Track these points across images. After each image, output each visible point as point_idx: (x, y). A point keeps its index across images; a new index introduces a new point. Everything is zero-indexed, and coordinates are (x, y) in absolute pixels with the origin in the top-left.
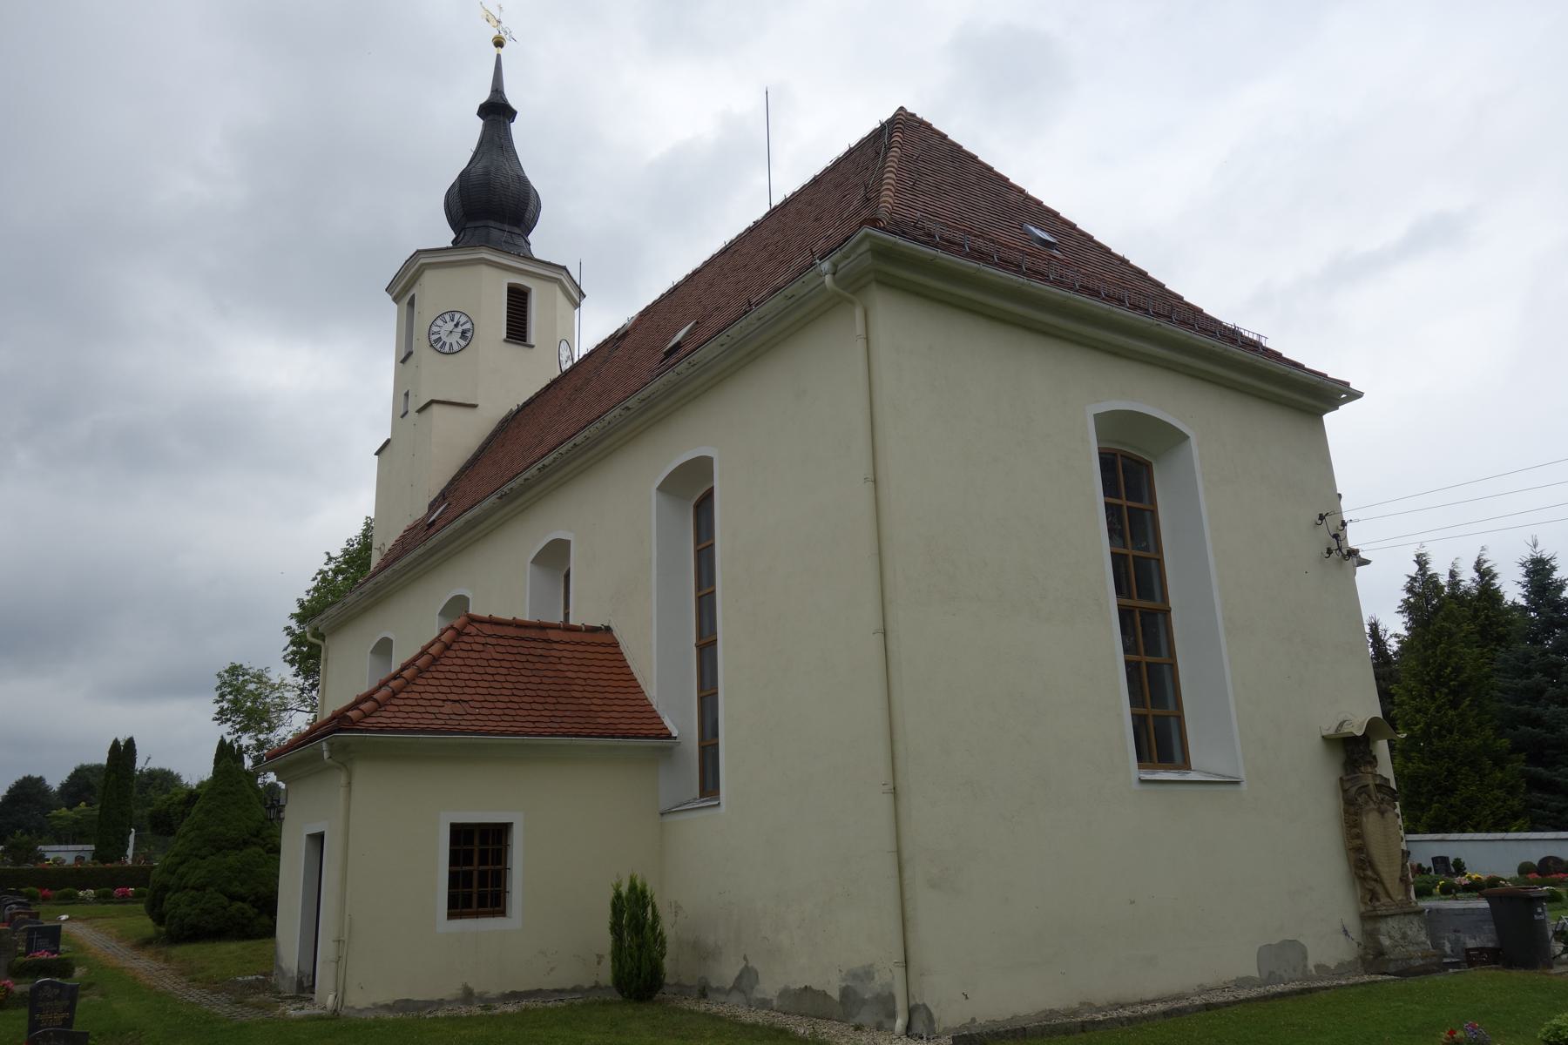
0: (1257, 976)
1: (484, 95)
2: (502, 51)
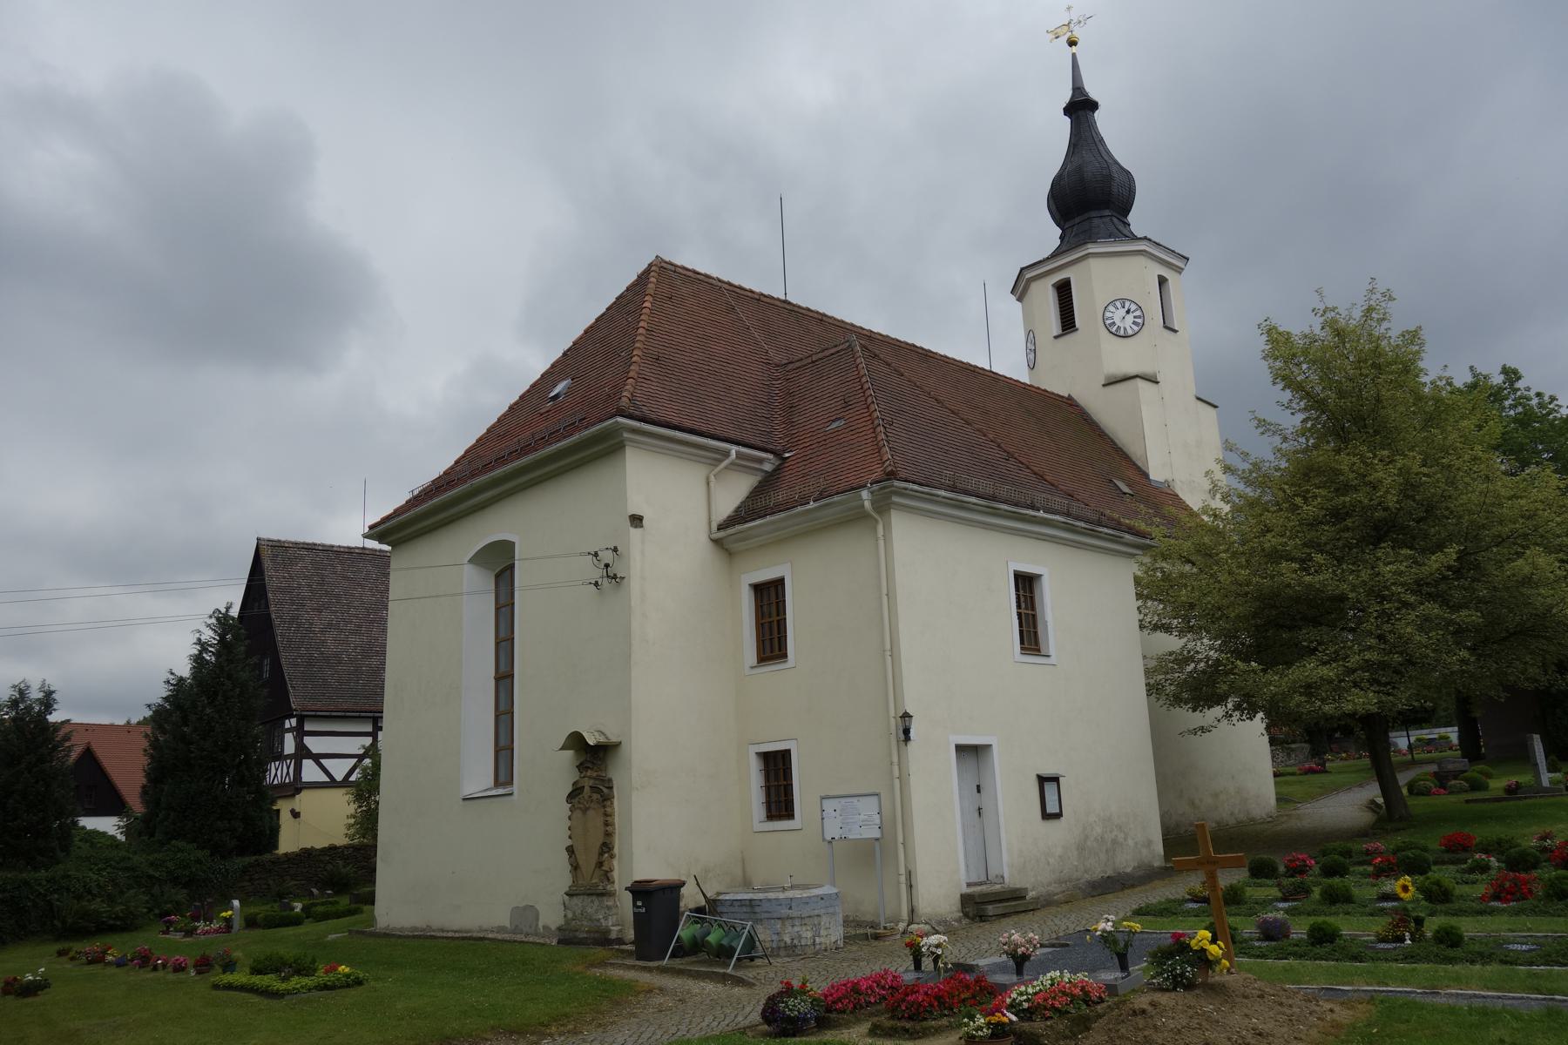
1: (1066, 95)
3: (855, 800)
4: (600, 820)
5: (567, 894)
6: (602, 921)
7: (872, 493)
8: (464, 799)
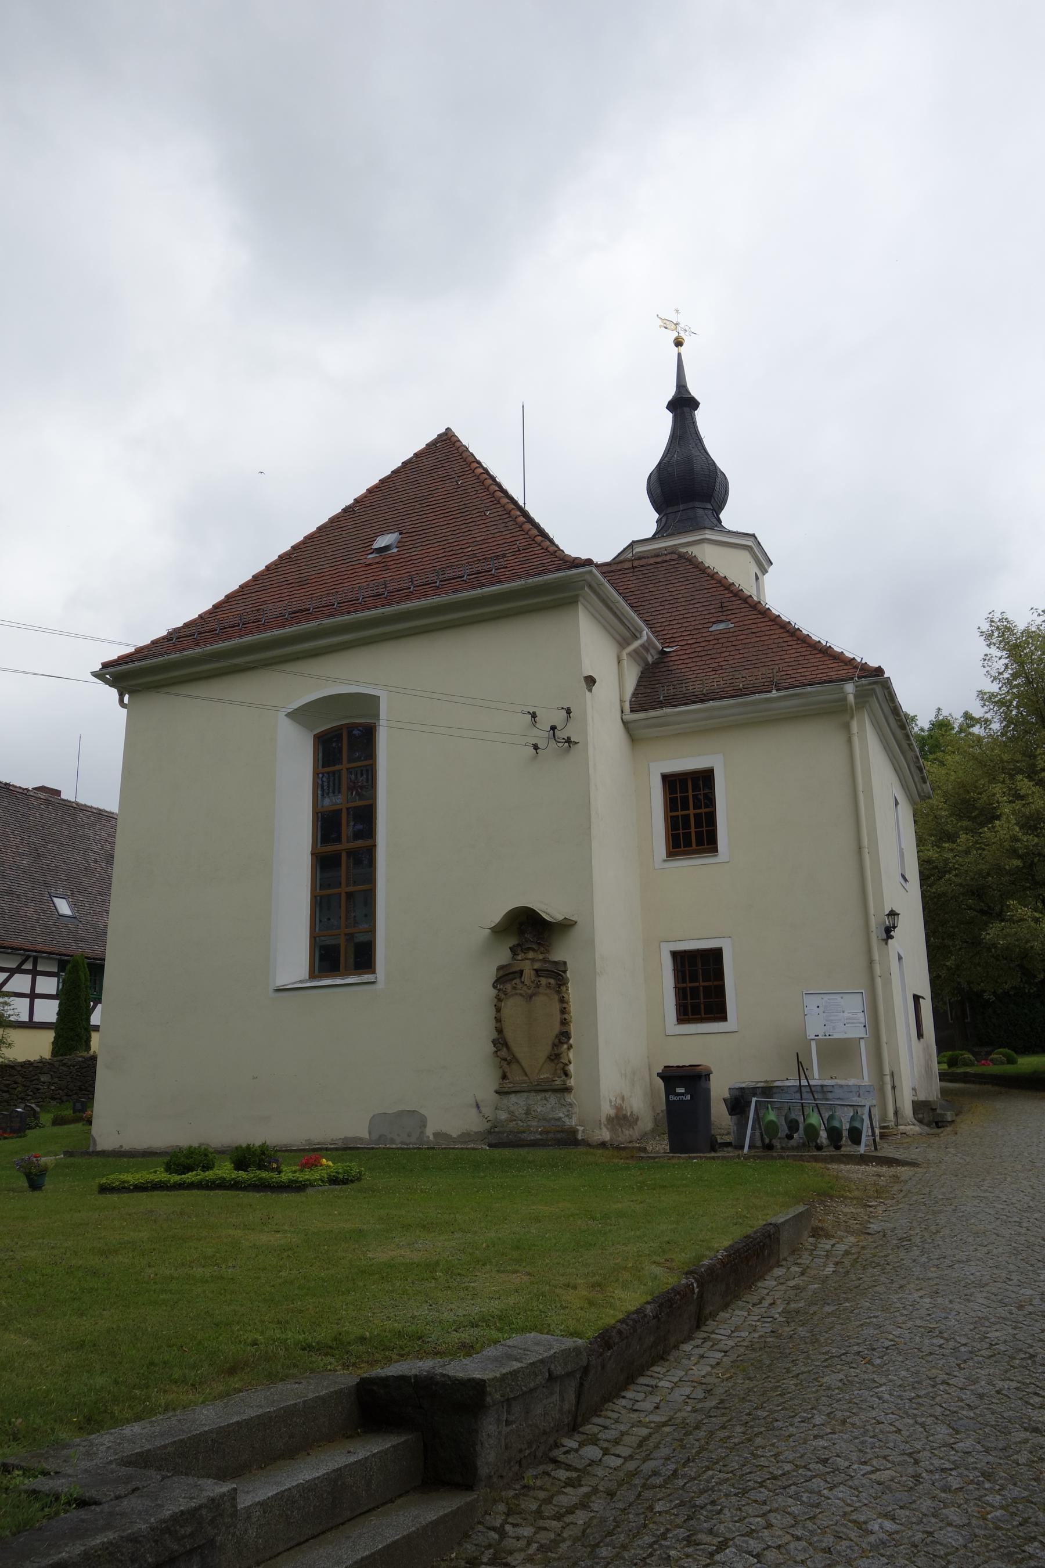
0: (367, 1136)
1: (670, 392)
2: (682, 349)
3: (838, 997)
4: (557, 1006)
5: (497, 1092)
6: (566, 1120)
7: (856, 687)
8: (278, 990)
